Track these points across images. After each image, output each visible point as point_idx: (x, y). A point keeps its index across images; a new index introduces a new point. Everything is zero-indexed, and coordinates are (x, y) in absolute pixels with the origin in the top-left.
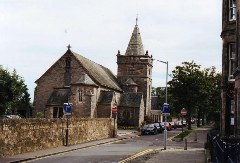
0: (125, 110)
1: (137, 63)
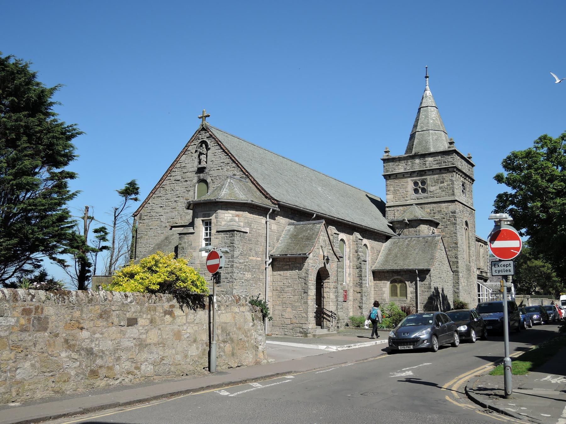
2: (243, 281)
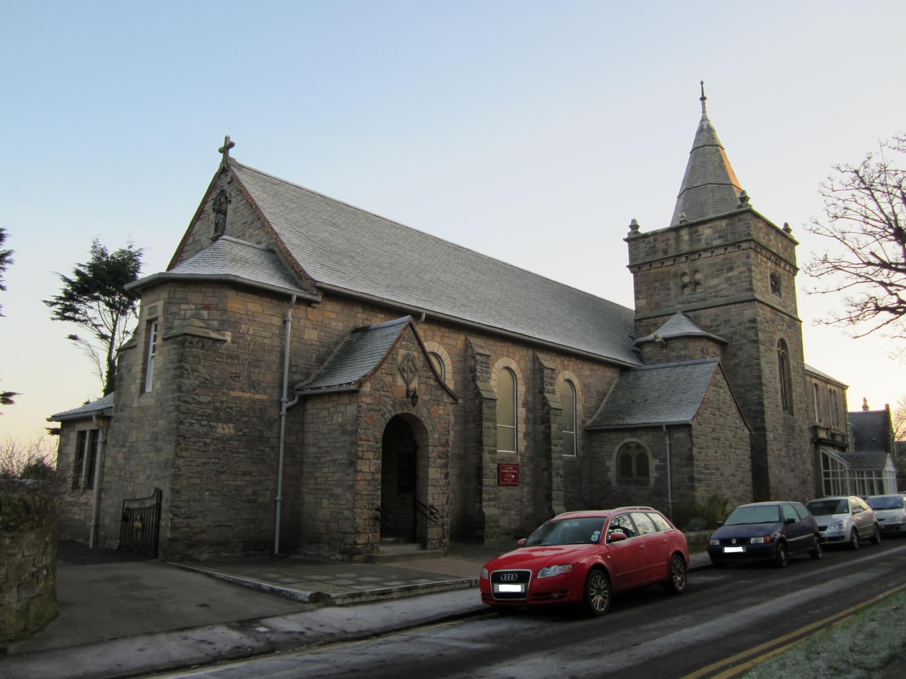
0: (627, 446)
1: (706, 250)
2: (208, 441)
